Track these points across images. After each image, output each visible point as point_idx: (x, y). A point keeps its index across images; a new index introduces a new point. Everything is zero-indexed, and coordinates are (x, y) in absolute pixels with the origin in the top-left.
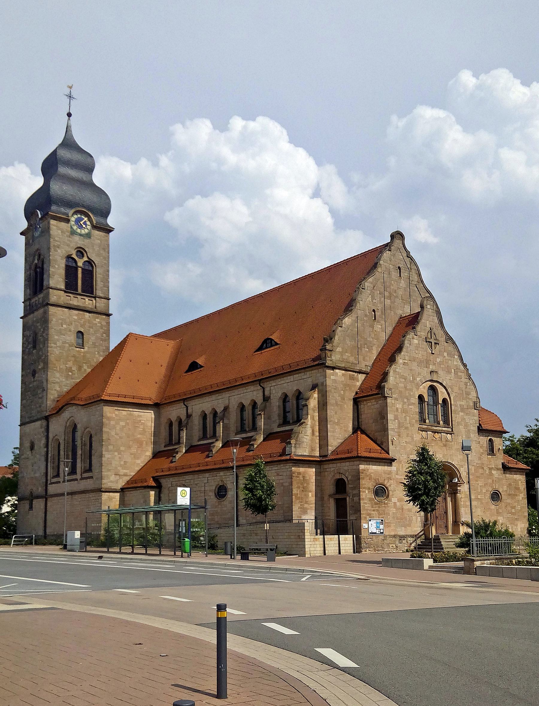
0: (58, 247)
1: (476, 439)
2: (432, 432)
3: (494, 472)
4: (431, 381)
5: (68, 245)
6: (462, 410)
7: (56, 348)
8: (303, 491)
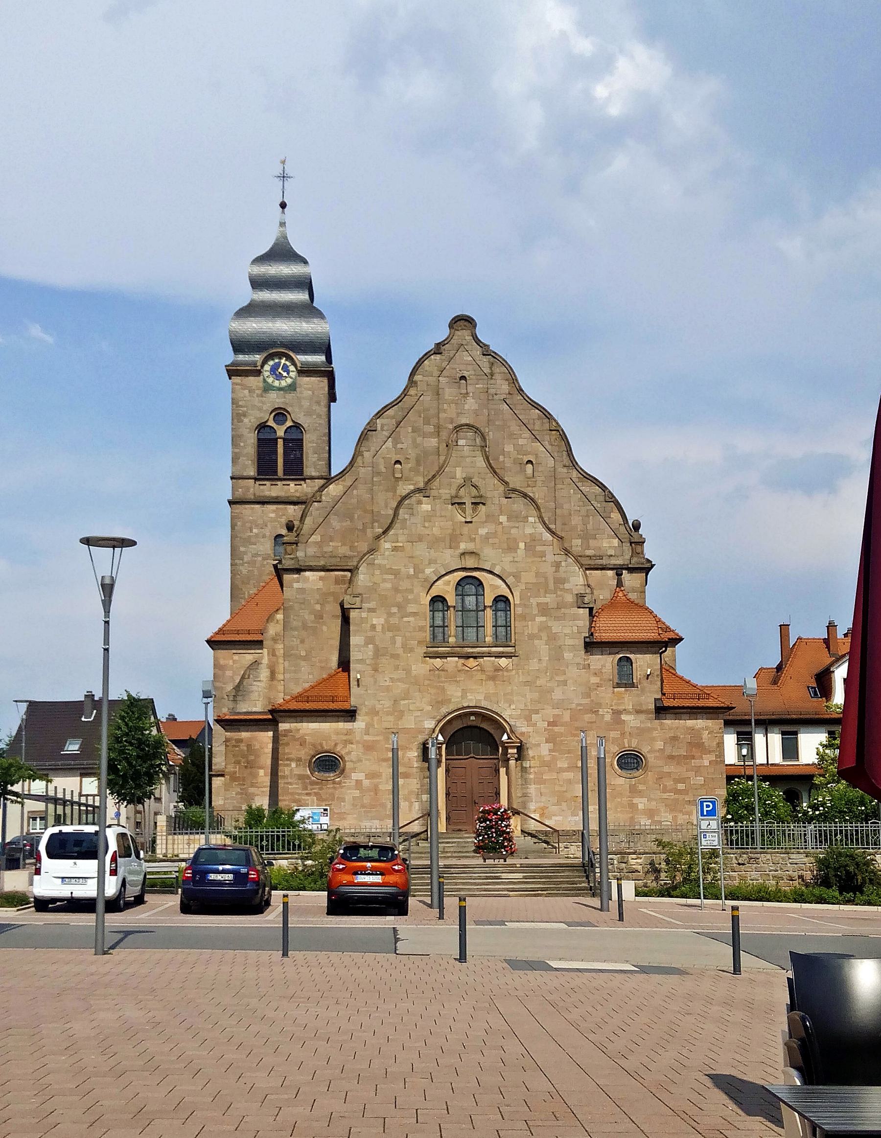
1: (578, 660)
2: (495, 657)
3: (624, 717)
4: (464, 569)
5: (260, 409)
6: (544, 610)
7: (242, 565)
8: (246, 767)
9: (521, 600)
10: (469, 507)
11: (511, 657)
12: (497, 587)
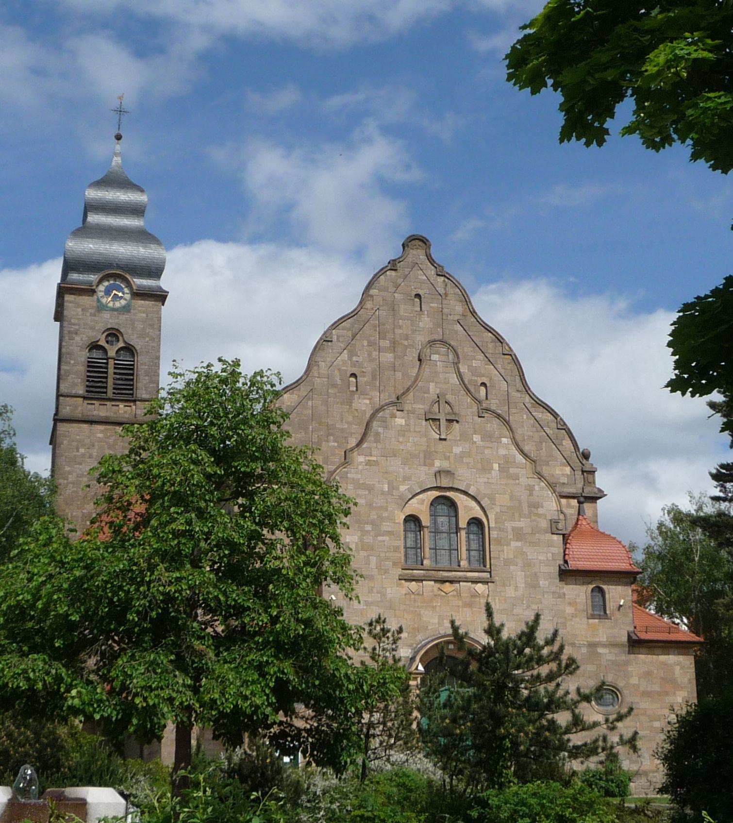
0: (76, 333)
1: (553, 589)
2: (472, 582)
3: (601, 650)
5: (92, 328)
6: (519, 535)
9: (496, 523)
10: (443, 423)
11: (487, 582)
12: (472, 509)
